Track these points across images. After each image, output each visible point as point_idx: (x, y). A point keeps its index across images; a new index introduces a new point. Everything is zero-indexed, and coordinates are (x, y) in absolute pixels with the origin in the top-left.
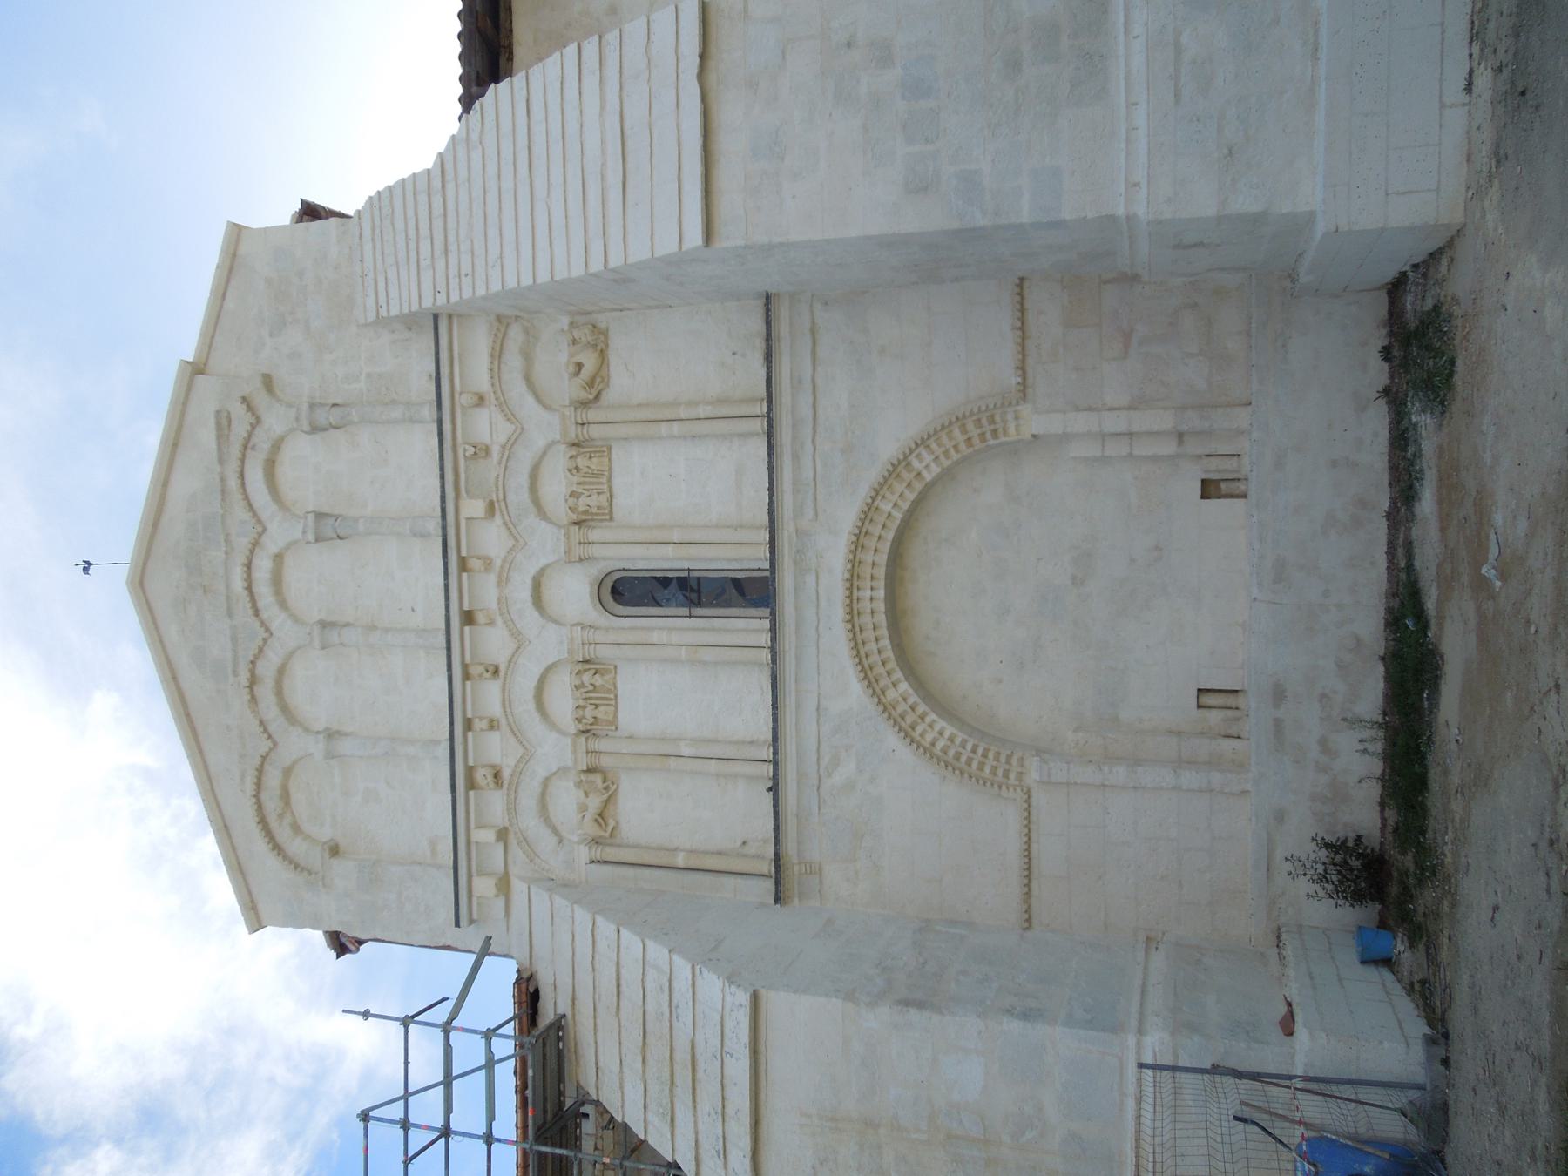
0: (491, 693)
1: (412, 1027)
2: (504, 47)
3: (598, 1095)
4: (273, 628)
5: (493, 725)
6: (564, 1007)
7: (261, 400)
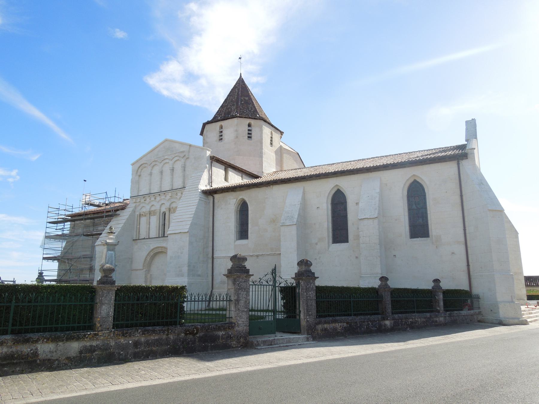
0: (153, 199)
1: (106, 193)
2: (64, 225)
3: (198, 200)
4: (161, 163)
5: (150, 199)
6: (121, 214)
7: (185, 158)
